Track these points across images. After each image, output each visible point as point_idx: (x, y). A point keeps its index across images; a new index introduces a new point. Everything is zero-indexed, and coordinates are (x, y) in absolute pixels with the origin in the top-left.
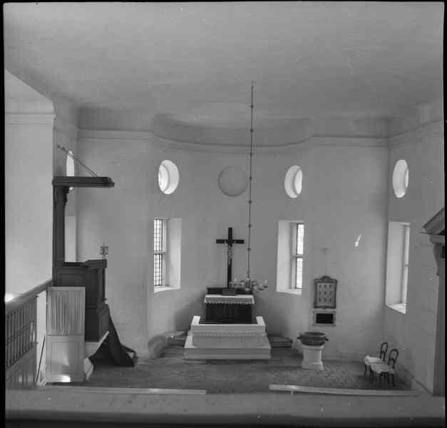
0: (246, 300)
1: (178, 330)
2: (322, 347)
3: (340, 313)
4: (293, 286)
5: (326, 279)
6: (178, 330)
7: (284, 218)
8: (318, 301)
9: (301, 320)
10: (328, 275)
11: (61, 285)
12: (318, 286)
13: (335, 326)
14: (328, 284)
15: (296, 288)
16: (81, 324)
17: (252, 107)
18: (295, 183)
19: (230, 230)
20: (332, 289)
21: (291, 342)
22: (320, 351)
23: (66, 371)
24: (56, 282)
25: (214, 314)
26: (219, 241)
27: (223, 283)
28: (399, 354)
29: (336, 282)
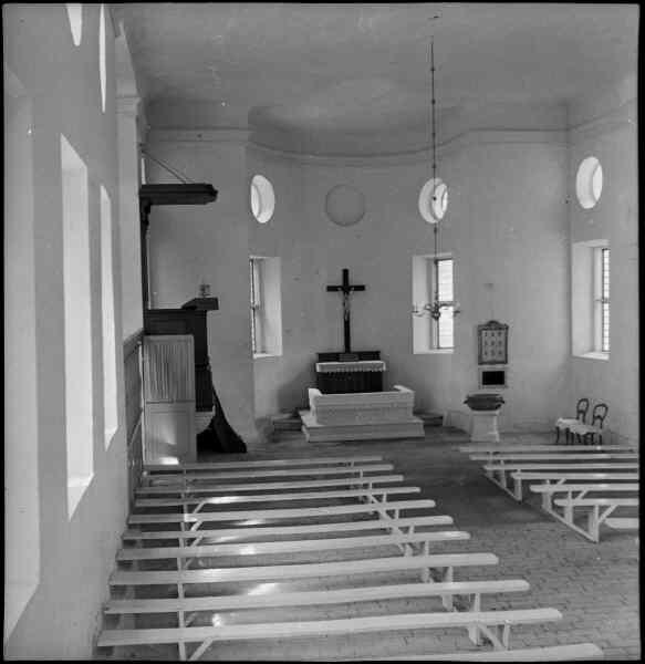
0: (375, 365)
1: (283, 411)
2: (497, 412)
3: (513, 371)
4: (435, 344)
5: (493, 325)
6: (283, 411)
7: (419, 253)
8: (484, 356)
9: (456, 385)
10: (495, 318)
11: (155, 334)
12: (484, 335)
13: (506, 387)
14: (496, 332)
15: (439, 348)
16: (190, 388)
17: (433, 70)
18: (436, 203)
19: (346, 272)
20: (502, 338)
21: (441, 418)
22: (495, 419)
23: (172, 452)
24: (147, 331)
25: (329, 384)
26: (331, 289)
27: (339, 346)
28: (609, 409)
29: (507, 328)
